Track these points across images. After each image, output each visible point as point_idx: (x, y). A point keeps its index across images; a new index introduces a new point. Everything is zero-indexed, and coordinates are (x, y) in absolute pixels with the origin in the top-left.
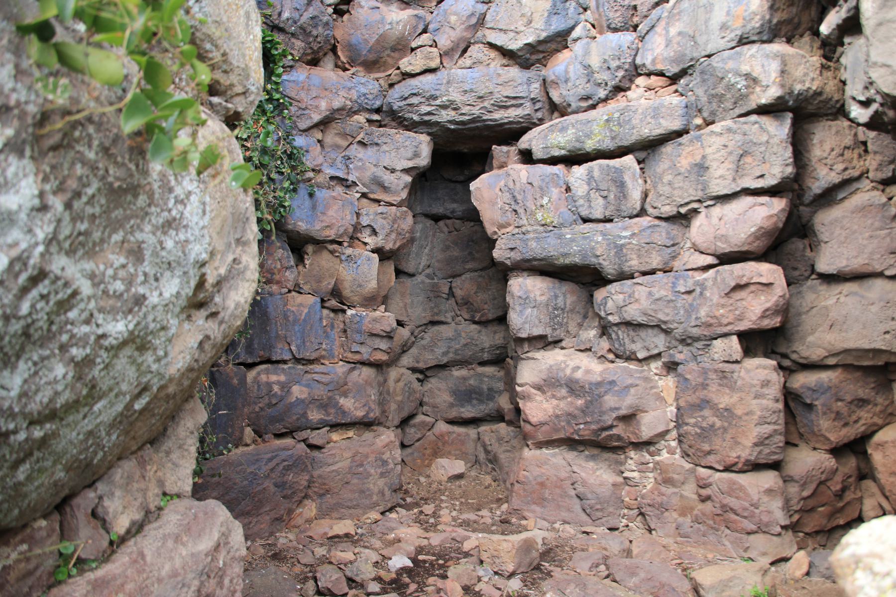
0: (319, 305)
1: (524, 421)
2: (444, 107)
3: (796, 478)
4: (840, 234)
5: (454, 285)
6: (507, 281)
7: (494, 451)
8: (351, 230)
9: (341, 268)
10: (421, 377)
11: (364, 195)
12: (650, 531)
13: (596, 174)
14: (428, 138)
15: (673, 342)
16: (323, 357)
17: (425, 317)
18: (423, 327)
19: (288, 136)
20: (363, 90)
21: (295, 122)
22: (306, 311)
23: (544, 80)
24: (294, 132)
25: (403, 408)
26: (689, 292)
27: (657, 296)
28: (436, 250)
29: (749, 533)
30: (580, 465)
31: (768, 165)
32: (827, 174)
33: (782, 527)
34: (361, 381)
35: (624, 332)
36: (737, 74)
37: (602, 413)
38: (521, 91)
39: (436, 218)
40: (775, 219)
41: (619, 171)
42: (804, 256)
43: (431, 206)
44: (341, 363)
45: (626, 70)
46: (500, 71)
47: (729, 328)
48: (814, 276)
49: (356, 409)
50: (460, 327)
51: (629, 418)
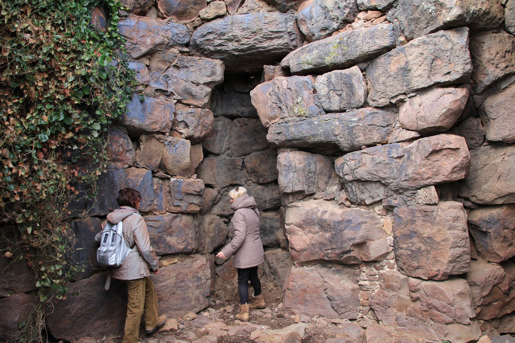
0: (150, 175)
1: (291, 248)
2: (230, 40)
3: (478, 283)
4: (504, 113)
5: (245, 160)
6: (277, 155)
7: (275, 267)
8: (170, 124)
9: (165, 150)
10: (226, 220)
11: (179, 101)
12: (378, 321)
13: (333, 79)
14: (221, 62)
15: (390, 192)
16: (155, 210)
17: (227, 182)
18: (226, 188)
19: (124, 62)
20: (176, 31)
21: (129, 53)
22: (141, 179)
23: (296, 20)
24: (129, 60)
25: (215, 241)
26: (400, 157)
27: (378, 161)
28: (232, 138)
29: (447, 324)
30: (329, 277)
31: (453, 65)
32: (494, 71)
33: (471, 319)
34: (181, 225)
35: (356, 187)
37: (343, 242)
38: (281, 27)
39: (232, 118)
40: (459, 103)
41: (349, 77)
42: (478, 129)
43: (228, 109)
44: (168, 213)
45: (351, 8)
46: (267, 14)
47: (429, 180)
48: (485, 144)
49: (178, 244)
50: (250, 187)
51: (361, 245)
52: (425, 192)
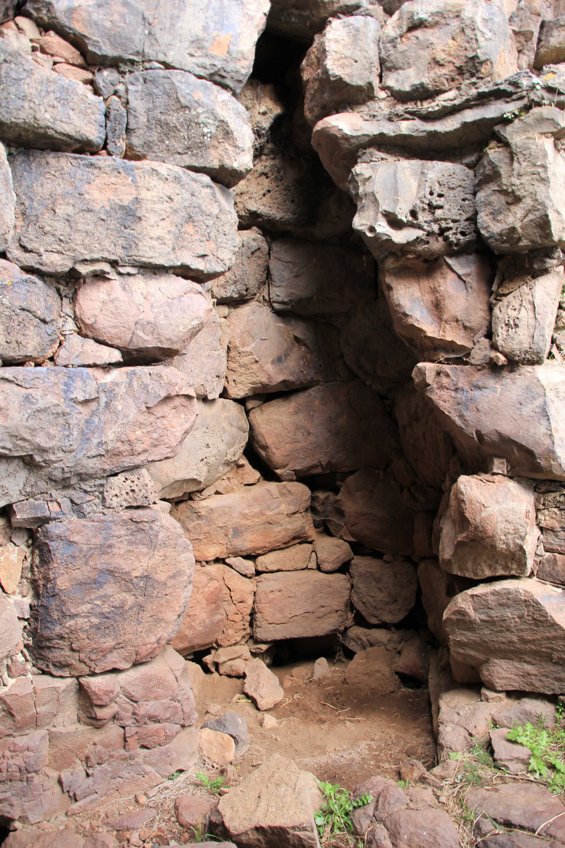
27: (41, 404)
36: (213, 113)
52: (129, 482)
